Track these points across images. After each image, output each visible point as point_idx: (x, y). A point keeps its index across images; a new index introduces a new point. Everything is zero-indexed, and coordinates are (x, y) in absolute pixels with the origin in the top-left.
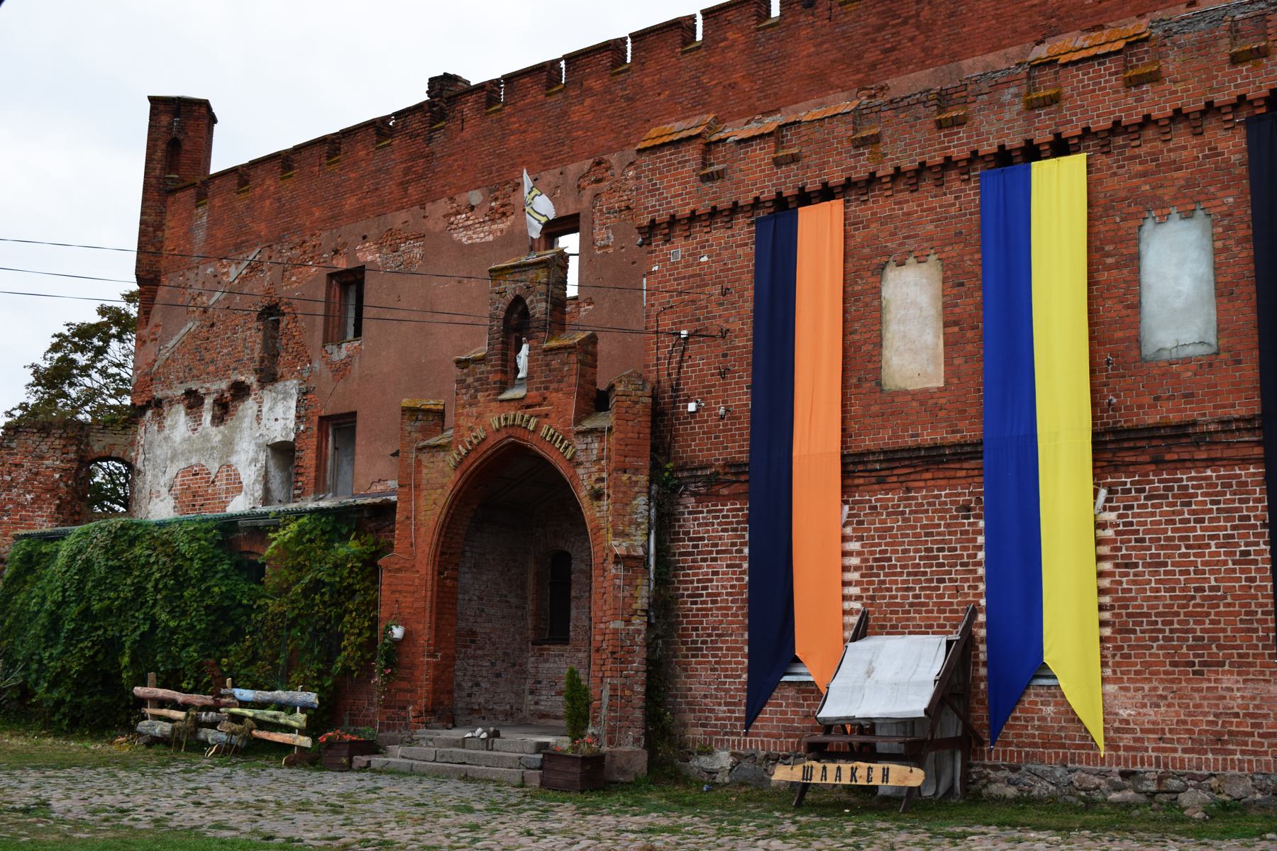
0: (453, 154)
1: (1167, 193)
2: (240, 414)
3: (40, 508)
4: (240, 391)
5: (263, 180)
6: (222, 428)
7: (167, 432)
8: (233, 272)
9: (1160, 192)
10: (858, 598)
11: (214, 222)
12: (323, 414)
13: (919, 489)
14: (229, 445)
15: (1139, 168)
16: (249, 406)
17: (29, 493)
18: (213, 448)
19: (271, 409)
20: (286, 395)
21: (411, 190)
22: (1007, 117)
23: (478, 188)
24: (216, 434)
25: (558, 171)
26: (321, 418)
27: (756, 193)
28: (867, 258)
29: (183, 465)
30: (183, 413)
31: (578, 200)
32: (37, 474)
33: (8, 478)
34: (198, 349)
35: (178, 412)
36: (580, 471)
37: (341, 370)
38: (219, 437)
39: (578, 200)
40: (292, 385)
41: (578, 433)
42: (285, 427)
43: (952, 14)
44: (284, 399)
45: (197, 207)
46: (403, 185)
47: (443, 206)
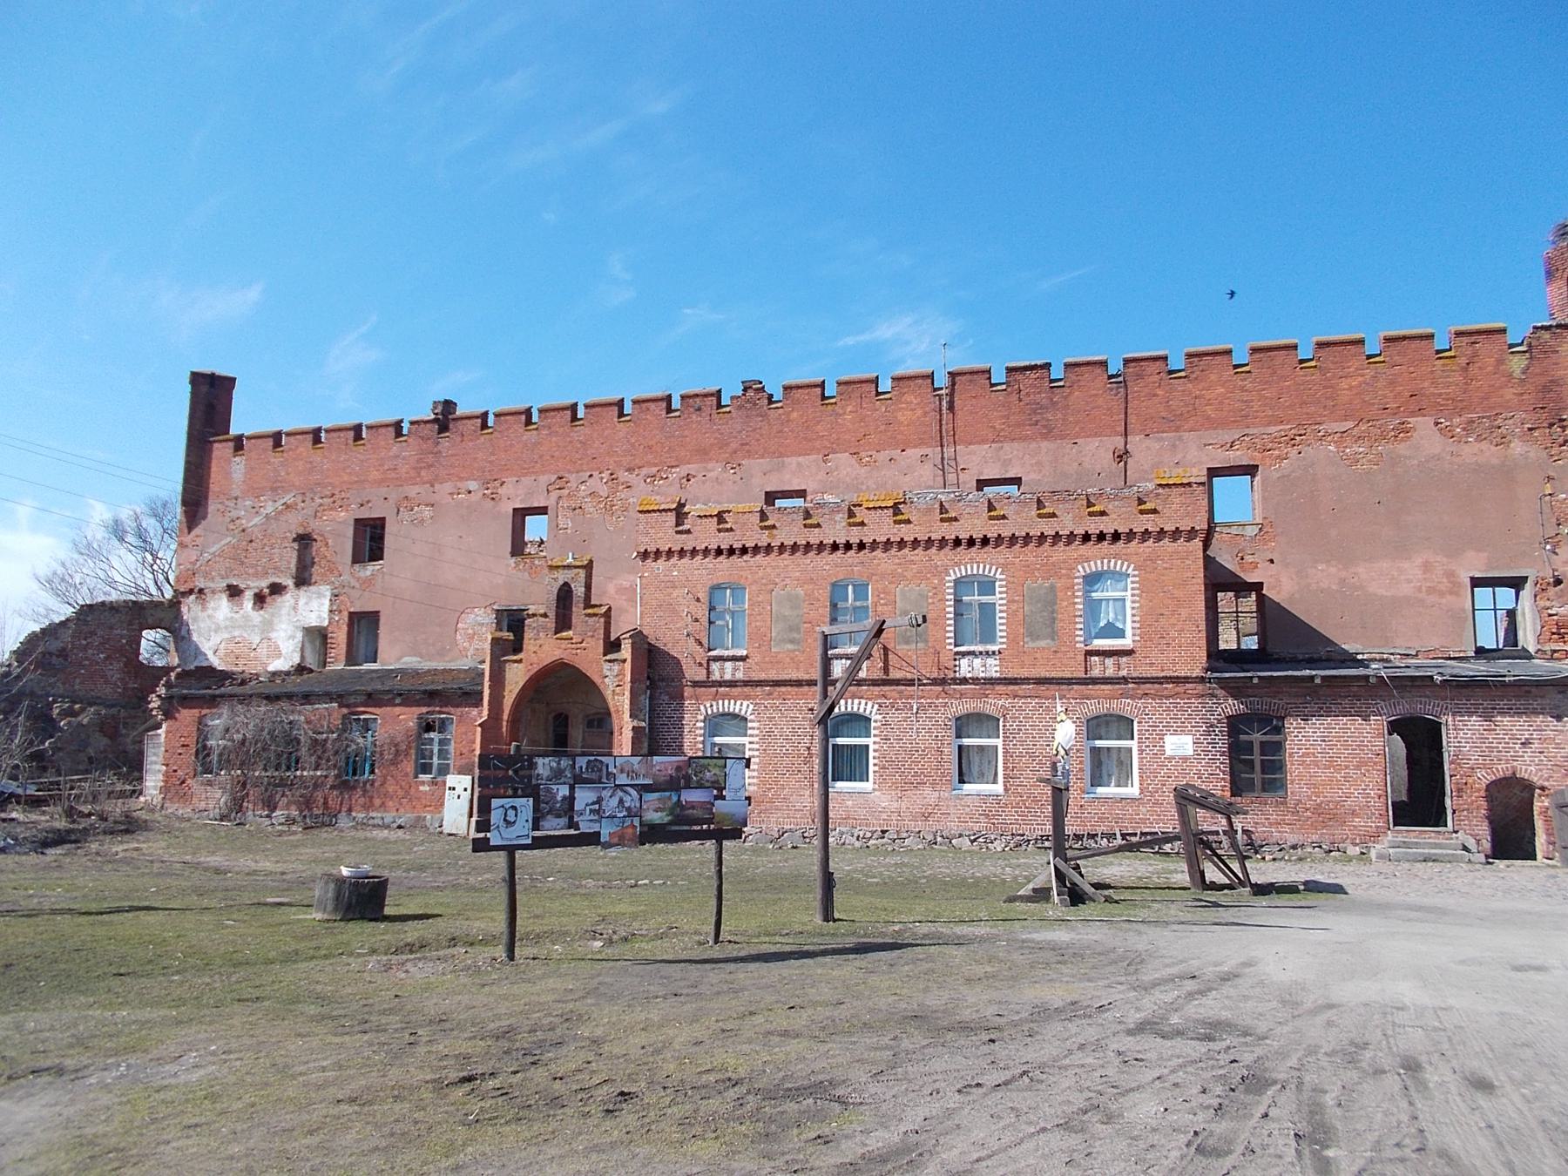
0: (455, 455)
1: (909, 575)
2: (279, 604)
3: (111, 664)
4: (277, 589)
5: (297, 447)
6: (262, 612)
7: (210, 612)
8: (270, 508)
9: (905, 573)
10: (758, 750)
11: (250, 470)
12: (352, 610)
13: (789, 700)
14: (268, 626)
15: (897, 561)
16: (287, 599)
17: (102, 653)
18: (255, 626)
19: (306, 603)
20: (320, 595)
21: (423, 473)
22: (838, 527)
23: (475, 480)
24: (257, 617)
25: (533, 478)
26: (351, 614)
27: (706, 544)
28: (765, 585)
29: (226, 636)
30: (226, 599)
31: (547, 498)
32: (109, 639)
33: (84, 642)
34: (238, 557)
35: (220, 599)
36: (606, 680)
37: (368, 583)
38: (260, 619)
39: (547, 498)
40: (326, 591)
41: (606, 661)
42: (320, 617)
43: (781, 431)
44: (318, 597)
45: (235, 457)
46: (418, 470)
47: (448, 487)
